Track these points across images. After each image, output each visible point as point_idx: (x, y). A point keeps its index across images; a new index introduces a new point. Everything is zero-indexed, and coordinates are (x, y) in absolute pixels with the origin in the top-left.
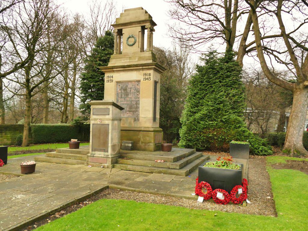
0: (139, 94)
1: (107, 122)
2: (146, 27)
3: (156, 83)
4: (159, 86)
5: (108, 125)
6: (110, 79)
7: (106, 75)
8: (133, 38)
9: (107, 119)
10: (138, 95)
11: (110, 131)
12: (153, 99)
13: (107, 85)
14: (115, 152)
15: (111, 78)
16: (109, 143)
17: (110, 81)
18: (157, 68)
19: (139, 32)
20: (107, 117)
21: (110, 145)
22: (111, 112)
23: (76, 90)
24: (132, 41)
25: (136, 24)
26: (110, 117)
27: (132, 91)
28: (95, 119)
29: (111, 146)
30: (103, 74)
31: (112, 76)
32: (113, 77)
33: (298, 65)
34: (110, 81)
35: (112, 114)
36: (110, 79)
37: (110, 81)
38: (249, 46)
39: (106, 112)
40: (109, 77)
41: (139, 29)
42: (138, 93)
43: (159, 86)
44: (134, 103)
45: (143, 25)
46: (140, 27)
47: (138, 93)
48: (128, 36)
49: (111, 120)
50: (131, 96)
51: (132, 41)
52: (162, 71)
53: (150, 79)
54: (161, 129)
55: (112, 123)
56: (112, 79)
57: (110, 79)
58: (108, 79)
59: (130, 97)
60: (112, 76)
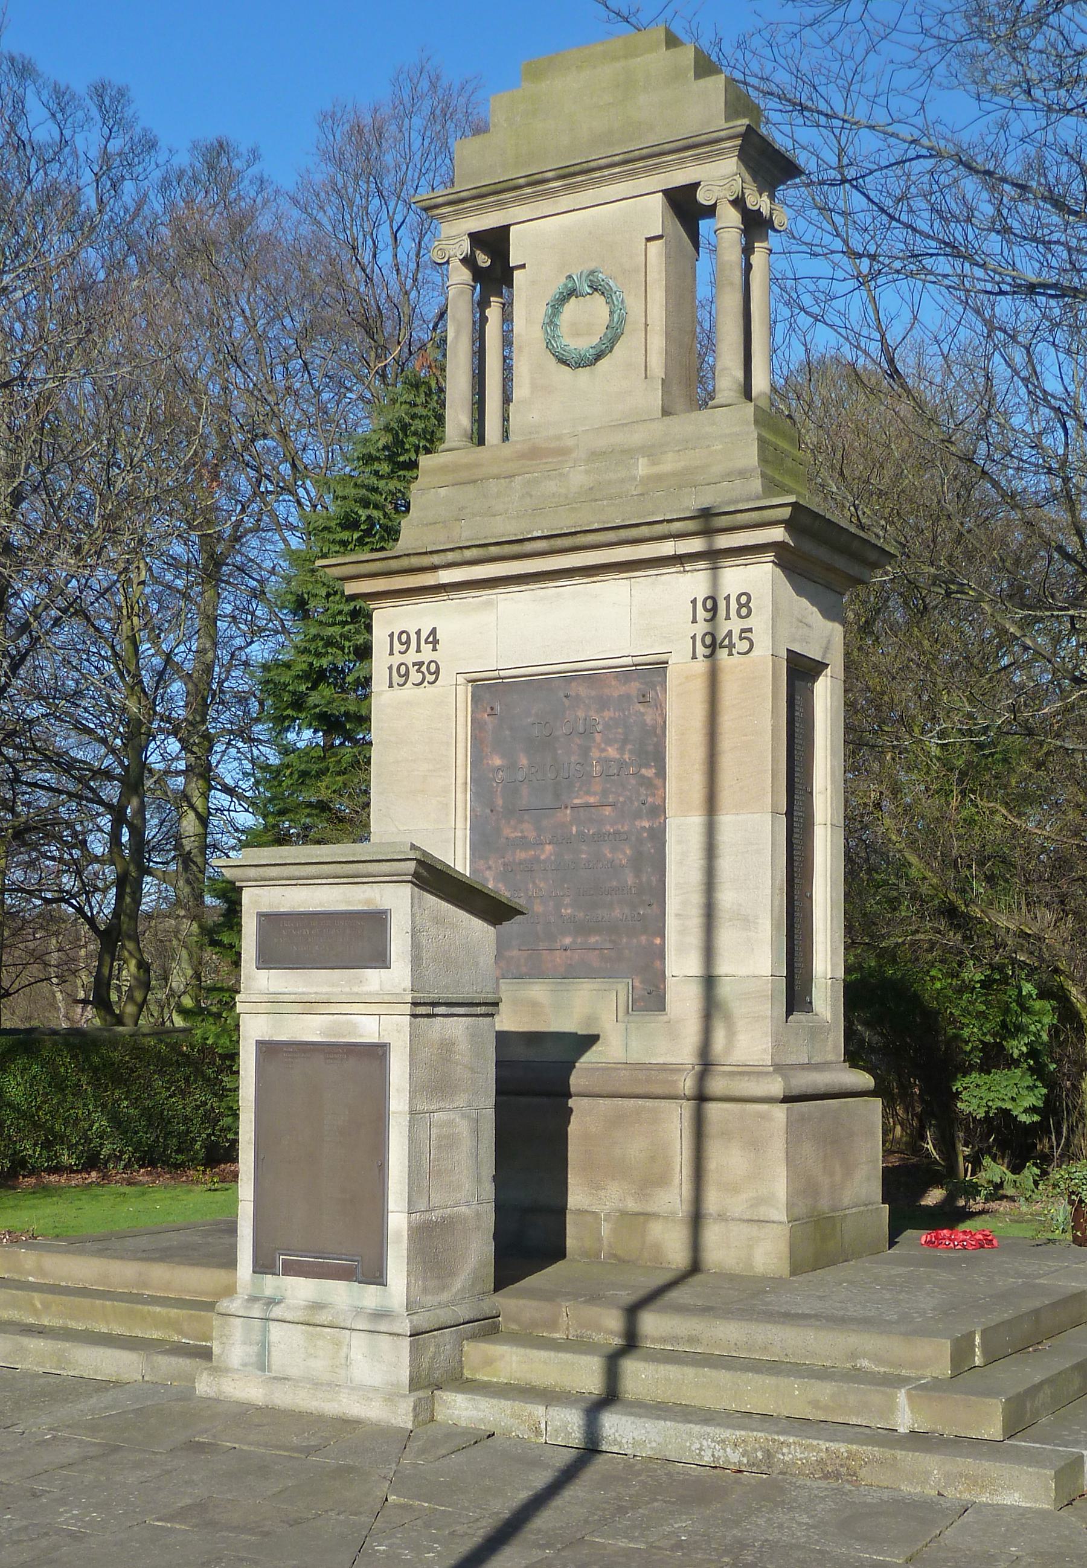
0: (662, 773)
1: (367, 1029)
2: (703, 197)
3: (801, 671)
4: (826, 696)
5: (378, 1053)
6: (412, 656)
7: (387, 621)
8: (599, 299)
9: (367, 1006)
10: (647, 783)
11: (398, 1103)
12: (774, 813)
13: (388, 704)
14: (443, 1288)
15: (426, 648)
16: (392, 1205)
17: (413, 671)
18: (822, 553)
19: (648, 240)
20: (373, 979)
21: (398, 1221)
22: (399, 944)
23: (219, 748)
24: (587, 317)
25: (614, 179)
26: (396, 977)
27: (595, 753)
28: (275, 1003)
29: (410, 1228)
30: (361, 618)
31: (434, 631)
32: (436, 642)
33: (86, 914)
34: (416, 677)
35: (416, 961)
36: (418, 658)
37: (416, 677)
38: (149, 1304)
39: (356, 940)
40: (408, 642)
41: (653, 212)
42: (649, 773)
43: (826, 696)
44: (624, 855)
45: (679, 178)
46: (657, 201)
47: (649, 773)
48: (558, 285)
49: (407, 1009)
50: (592, 800)
51: (587, 317)
52: (855, 570)
53: (744, 646)
54: (864, 1080)
55: (414, 1036)
56: (434, 656)
57: (412, 656)
58: (397, 659)
59: (587, 806)
60: (434, 631)
